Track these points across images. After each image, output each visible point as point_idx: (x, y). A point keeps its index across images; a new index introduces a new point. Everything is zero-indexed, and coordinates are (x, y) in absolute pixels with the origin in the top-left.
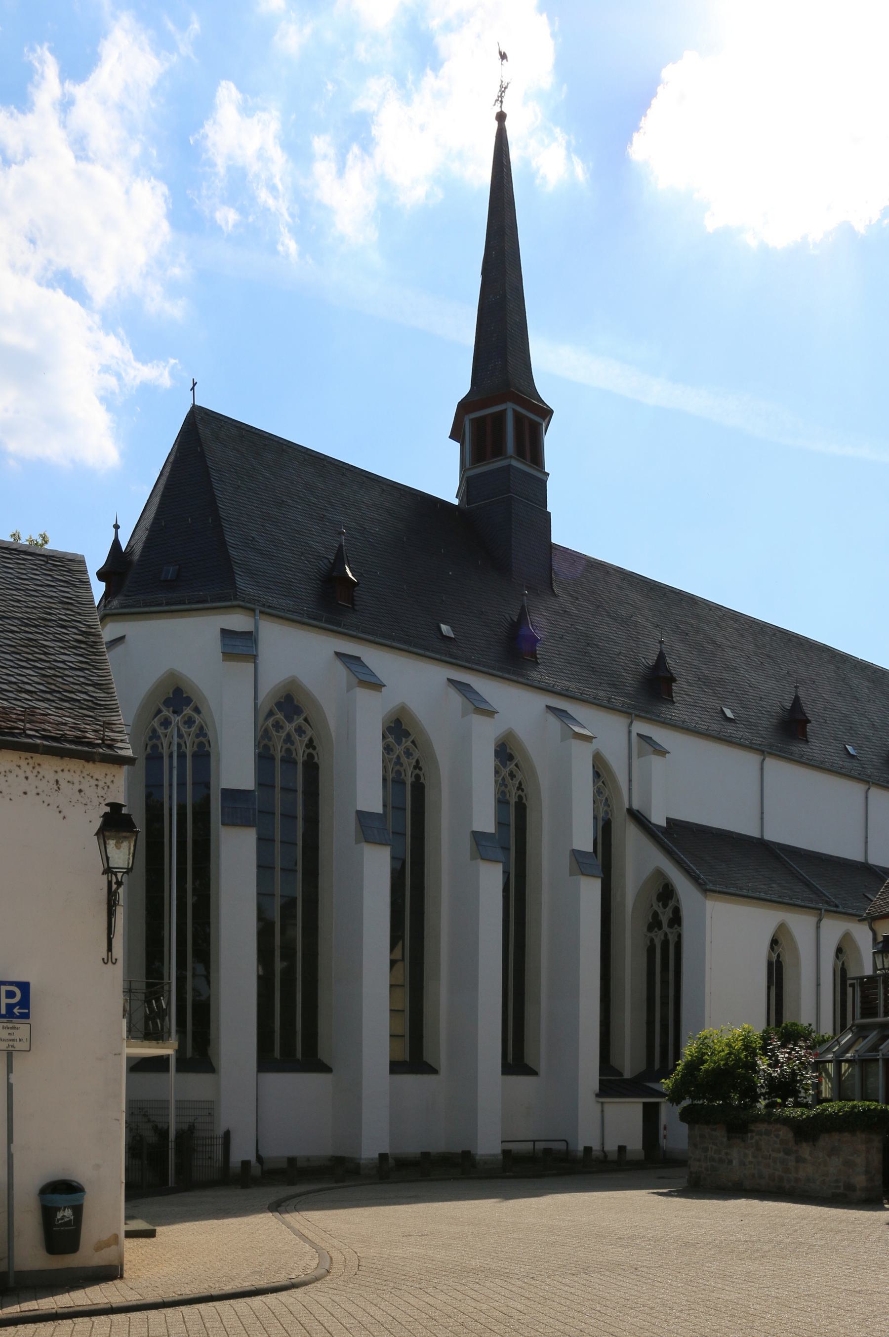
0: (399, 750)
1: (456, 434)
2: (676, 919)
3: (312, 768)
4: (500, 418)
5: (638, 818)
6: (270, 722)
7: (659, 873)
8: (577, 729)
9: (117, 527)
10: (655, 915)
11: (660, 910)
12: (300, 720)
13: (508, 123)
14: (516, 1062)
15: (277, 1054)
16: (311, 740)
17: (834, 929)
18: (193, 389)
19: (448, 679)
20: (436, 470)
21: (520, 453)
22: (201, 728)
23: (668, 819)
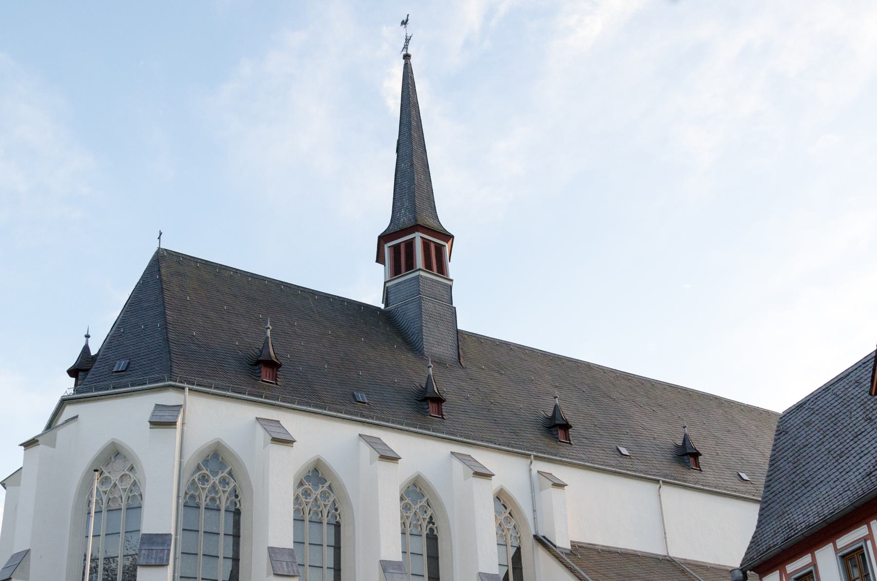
0: (416, 508)
1: (380, 259)
4: (410, 245)
5: (543, 542)
12: (225, 474)
13: (413, 61)
18: (159, 238)
19: (360, 435)
20: (366, 283)
21: (428, 266)
22: (135, 484)
23: (571, 542)
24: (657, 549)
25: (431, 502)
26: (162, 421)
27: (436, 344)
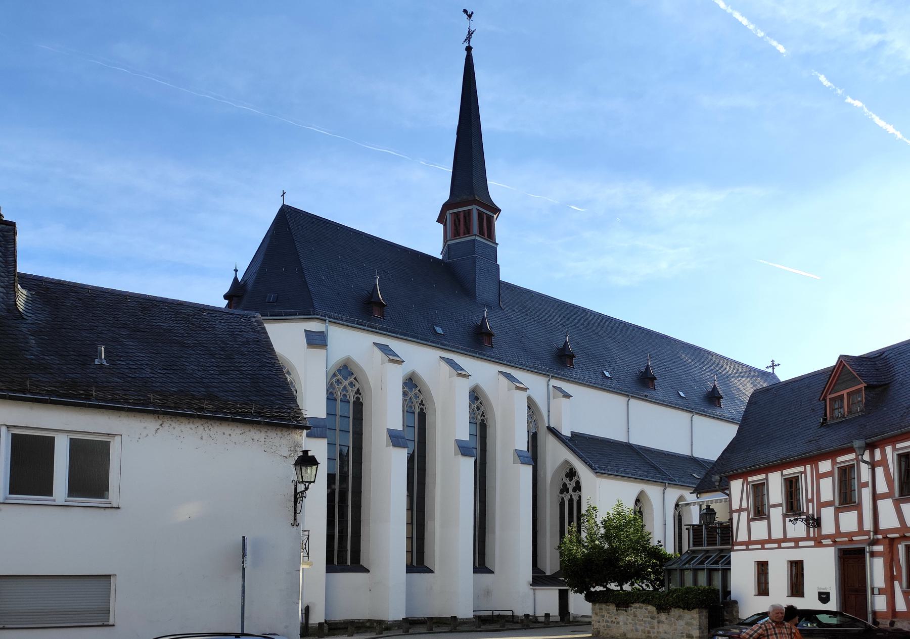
0: (411, 394)
2: (578, 487)
3: (358, 406)
4: (468, 214)
6: (334, 380)
7: (567, 462)
8: (518, 385)
9: (236, 270)
10: (565, 485)
11: (567, 482)
12: (352, 379)
13: (473, 51)
14: (481, 566)
15: (336, 562)
16: (358, 390)
17: (673, 494)
20: (430, 241)
21: (481, 233)
24: (622, 438)
25: (484, 402)
26: (316, 341)
27: (484, 291)
